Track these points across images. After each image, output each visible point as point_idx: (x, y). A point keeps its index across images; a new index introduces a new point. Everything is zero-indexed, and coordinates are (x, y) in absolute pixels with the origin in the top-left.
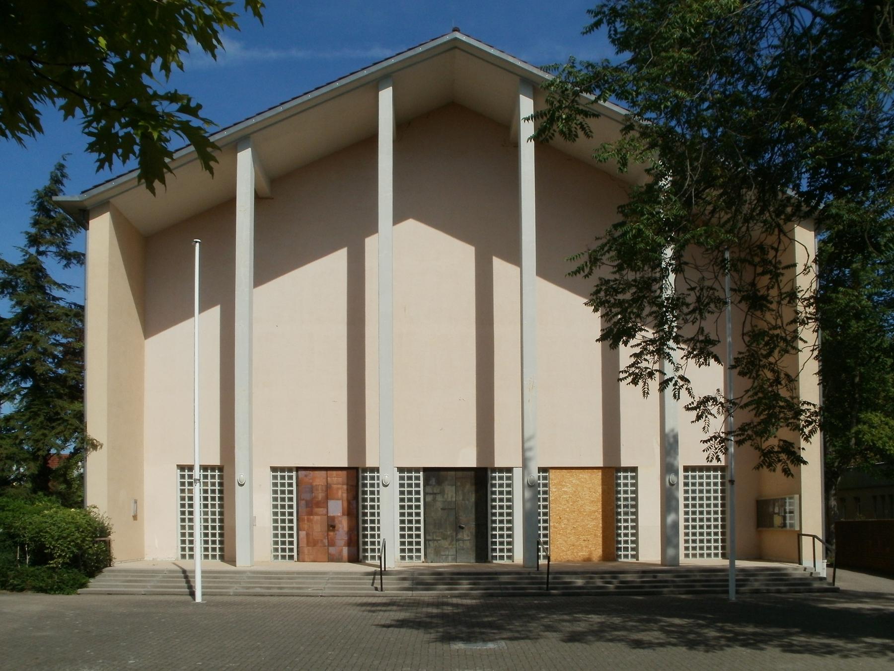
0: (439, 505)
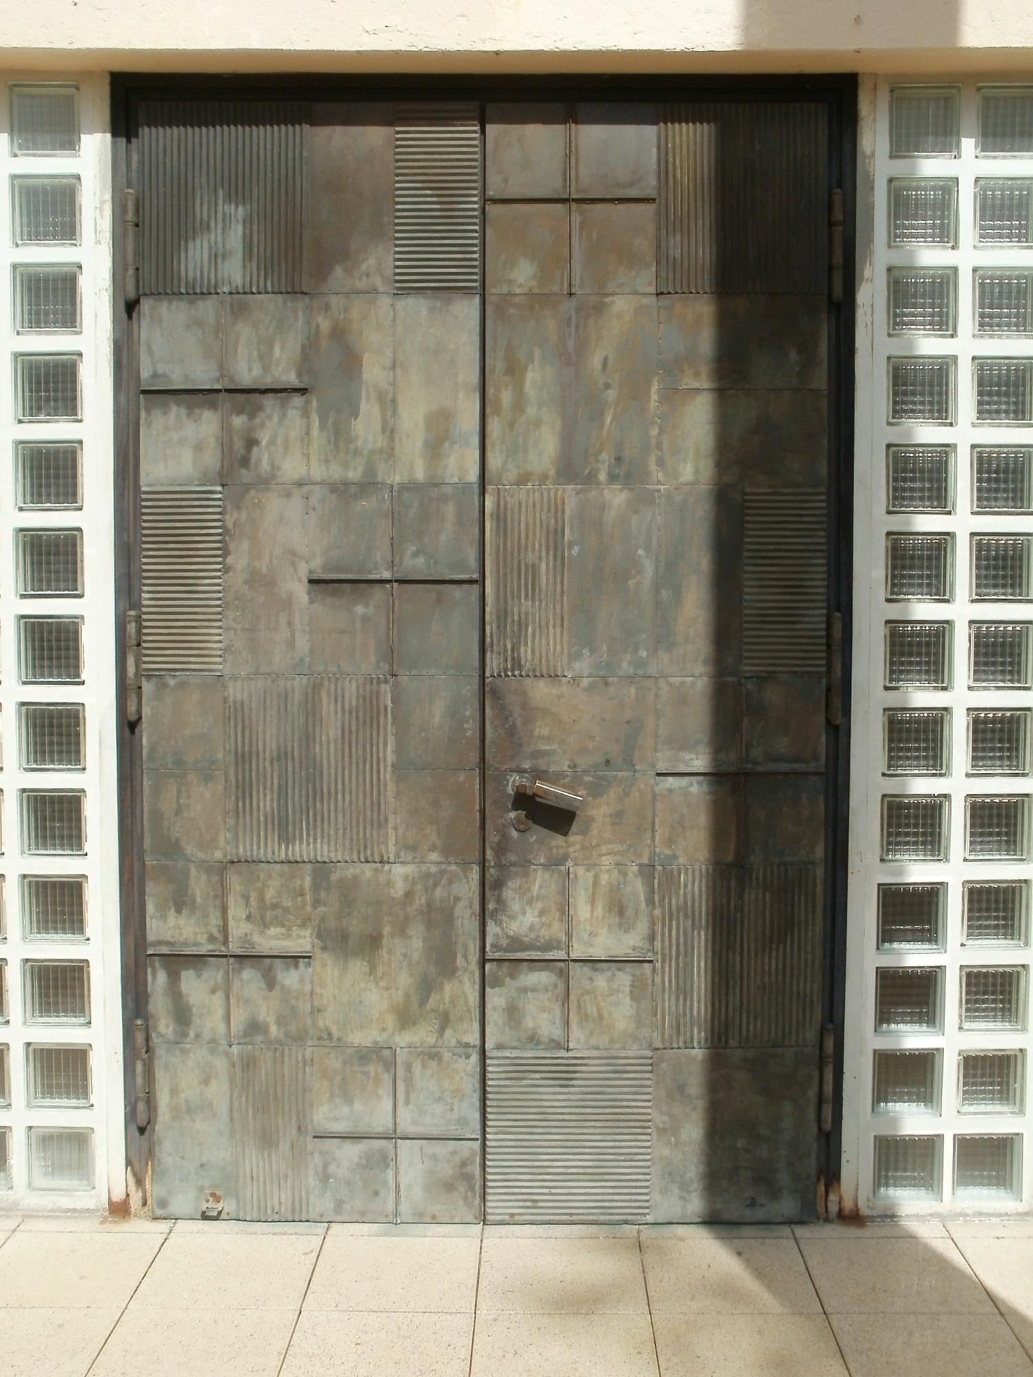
0: (290, 534)
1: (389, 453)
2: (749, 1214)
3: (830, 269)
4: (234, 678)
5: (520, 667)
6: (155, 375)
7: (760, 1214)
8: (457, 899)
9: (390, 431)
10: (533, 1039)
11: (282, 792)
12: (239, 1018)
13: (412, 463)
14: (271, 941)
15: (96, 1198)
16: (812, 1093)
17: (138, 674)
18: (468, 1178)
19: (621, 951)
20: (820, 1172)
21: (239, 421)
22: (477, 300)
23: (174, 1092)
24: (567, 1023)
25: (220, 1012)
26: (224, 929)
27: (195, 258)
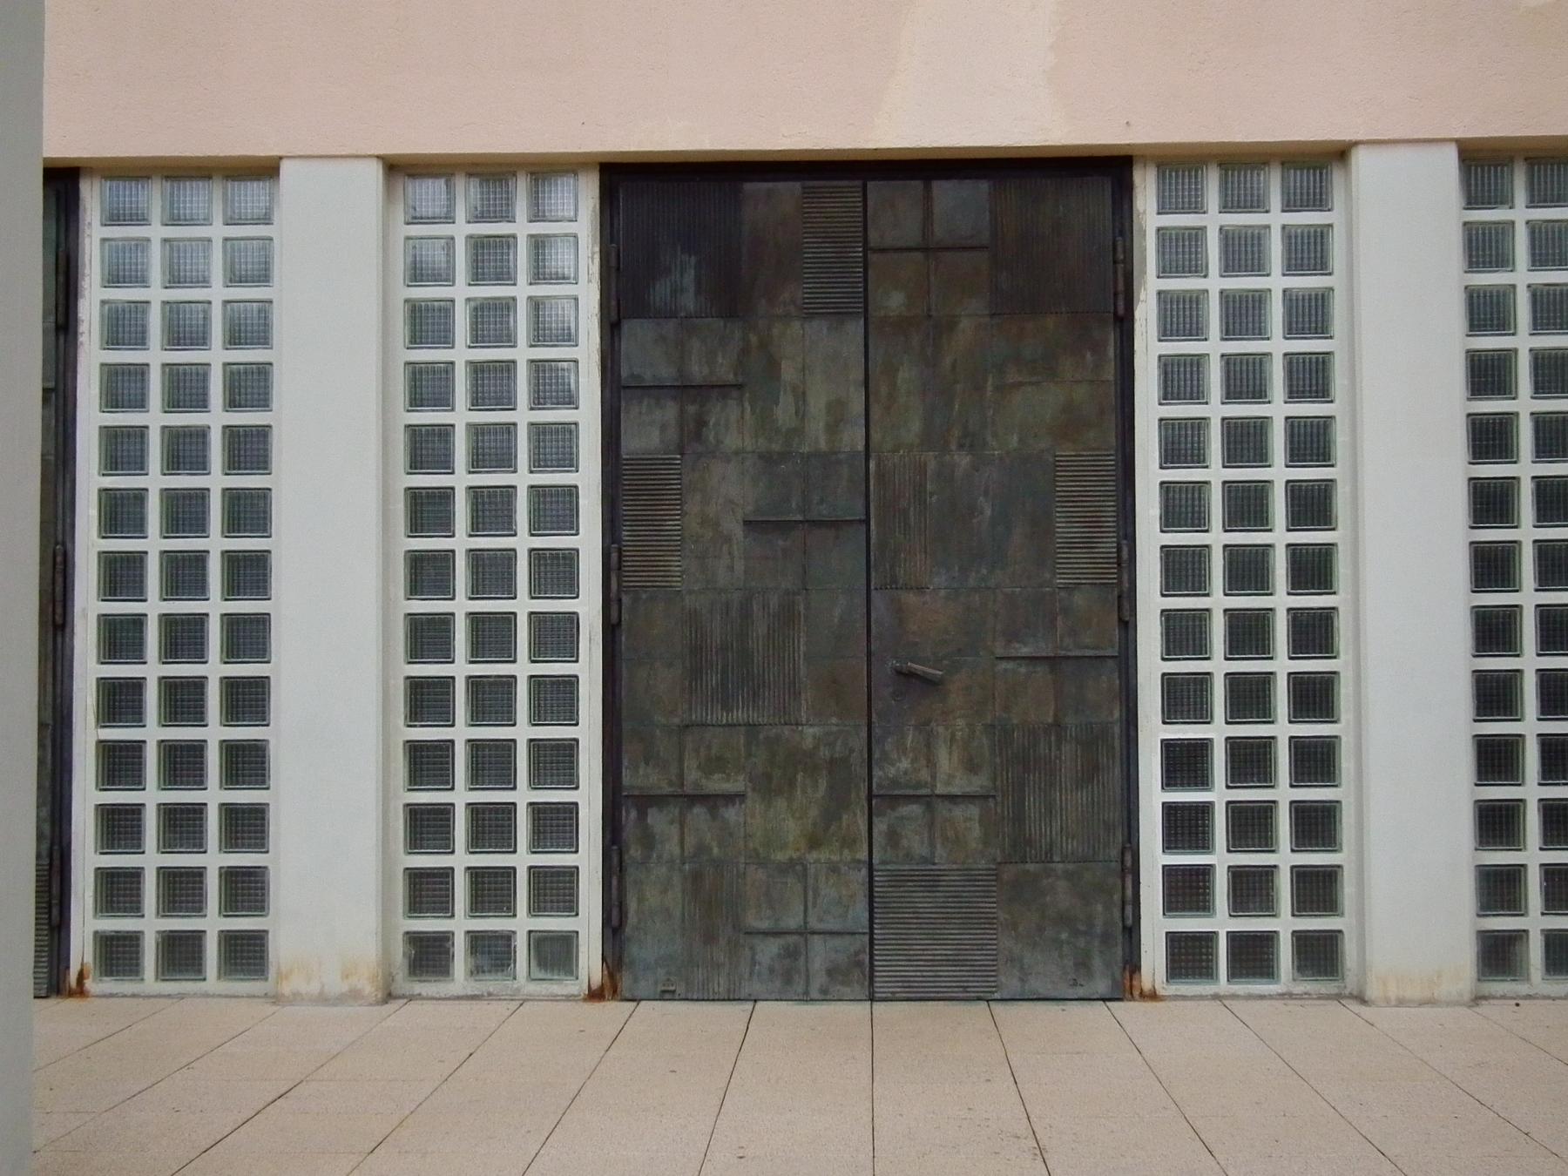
0: (728, 490)
1: (798, 432)
2: (1071, 993)
3: (1116, 295)
4: (690, 592)
5: (896, 582)
6: (632, 376)
7: (1081, 992)
8: (852, 751)
9: (801, 414)
10: (909, 857)
11: (724, 672)
12: (690, 841)
13: (817, 434)
14: (718, 784)
15: (578, 987)
16: (1117, 897)
17: (619, 591)
18: (859, 964)
19: (969, 790)
20: (1125, 963)
21: (692, 409)
22: (862, 322)
23: (641, 900)
24: (932, 845)
25: (676, 839)
26: (681, 776)
27: (661, 291)
